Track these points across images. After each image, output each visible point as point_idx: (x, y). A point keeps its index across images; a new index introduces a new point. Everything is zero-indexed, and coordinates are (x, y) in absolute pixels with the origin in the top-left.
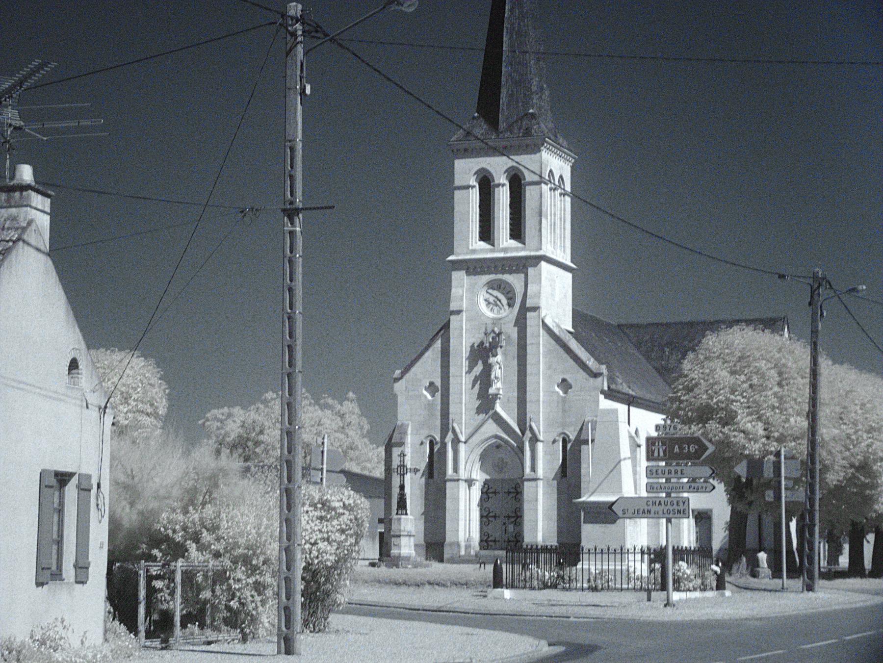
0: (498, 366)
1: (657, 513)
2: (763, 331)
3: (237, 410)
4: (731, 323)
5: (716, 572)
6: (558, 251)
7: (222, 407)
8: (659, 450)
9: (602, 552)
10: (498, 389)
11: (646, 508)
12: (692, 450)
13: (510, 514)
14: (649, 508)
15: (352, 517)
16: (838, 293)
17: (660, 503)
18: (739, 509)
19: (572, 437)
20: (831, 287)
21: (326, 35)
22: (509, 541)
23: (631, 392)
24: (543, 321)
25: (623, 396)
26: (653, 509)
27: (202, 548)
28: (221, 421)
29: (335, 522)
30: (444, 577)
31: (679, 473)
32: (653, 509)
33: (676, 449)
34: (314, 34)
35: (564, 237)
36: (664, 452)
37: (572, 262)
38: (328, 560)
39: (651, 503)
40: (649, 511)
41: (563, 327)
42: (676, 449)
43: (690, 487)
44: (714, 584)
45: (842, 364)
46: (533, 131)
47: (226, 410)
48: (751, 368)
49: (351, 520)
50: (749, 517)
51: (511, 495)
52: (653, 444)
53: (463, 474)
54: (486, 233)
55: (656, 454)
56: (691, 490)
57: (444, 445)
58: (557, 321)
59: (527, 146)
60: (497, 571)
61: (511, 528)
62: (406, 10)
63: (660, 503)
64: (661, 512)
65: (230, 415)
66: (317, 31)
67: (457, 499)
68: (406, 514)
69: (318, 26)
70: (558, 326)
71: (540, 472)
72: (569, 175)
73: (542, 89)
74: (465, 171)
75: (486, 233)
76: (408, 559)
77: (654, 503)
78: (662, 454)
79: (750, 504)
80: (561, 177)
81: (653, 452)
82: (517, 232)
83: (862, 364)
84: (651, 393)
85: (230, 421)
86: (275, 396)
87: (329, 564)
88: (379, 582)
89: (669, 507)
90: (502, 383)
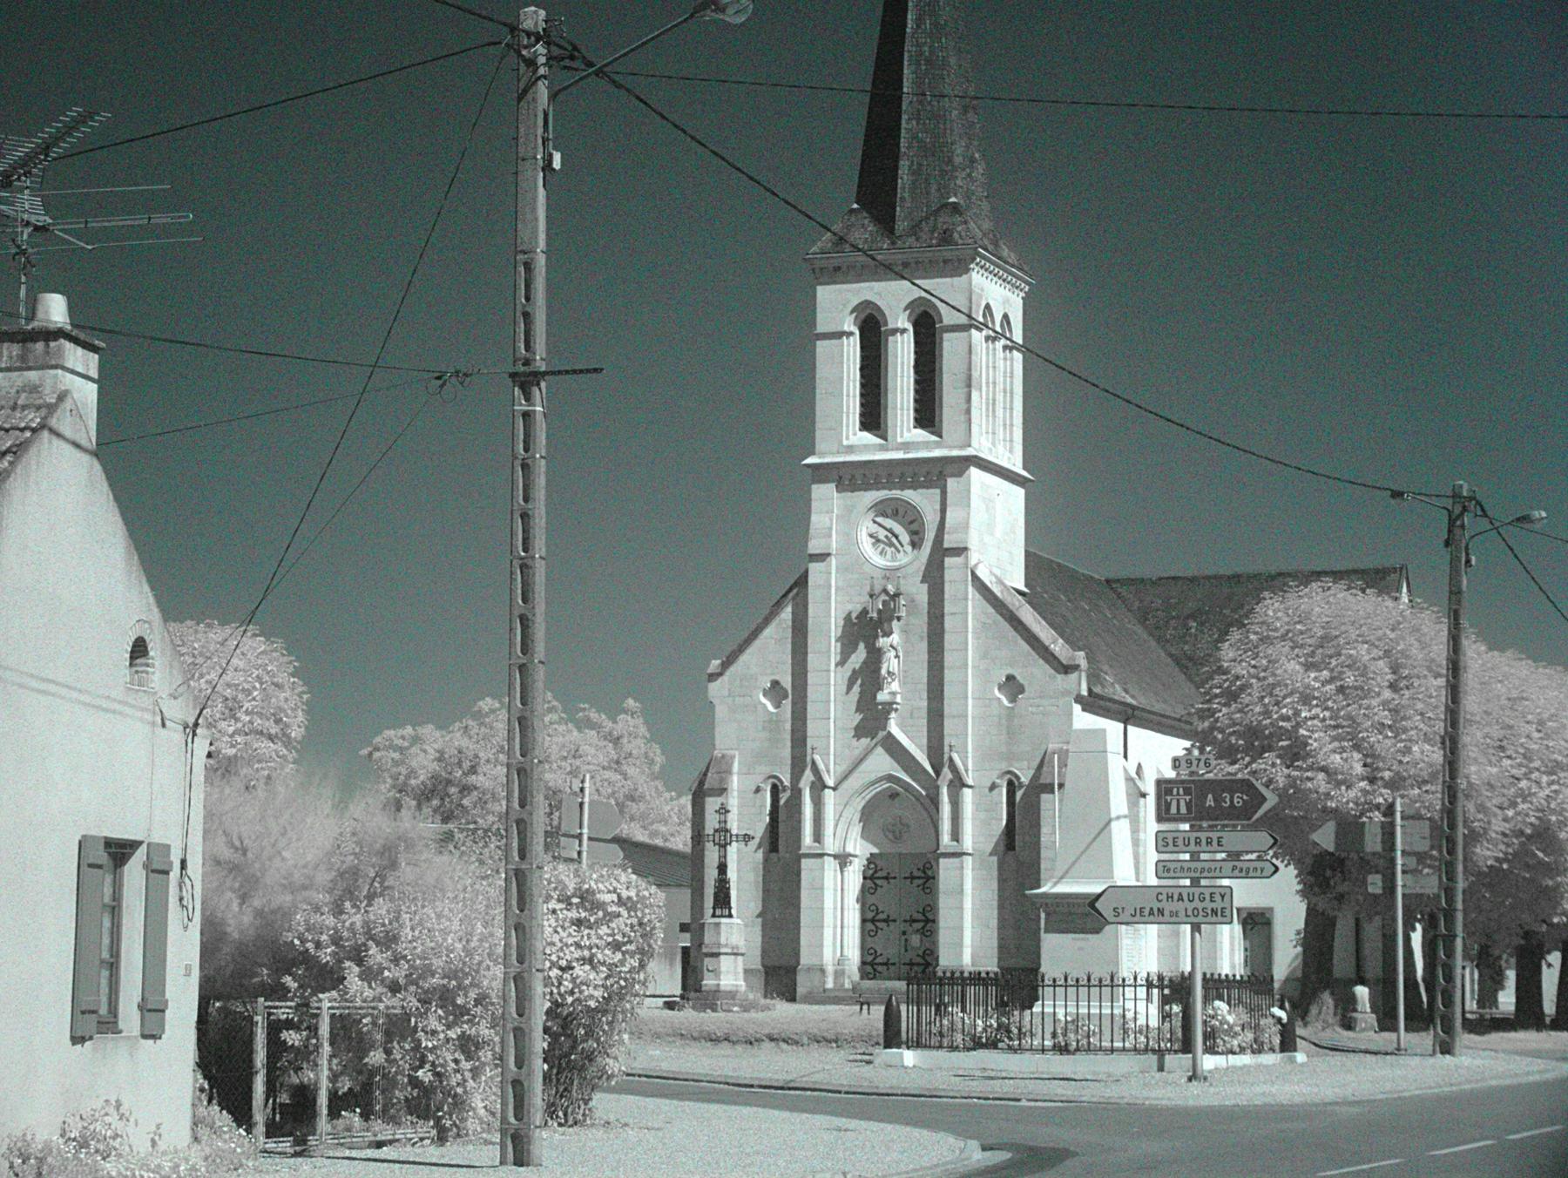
0: (893, 653)
3: (428, 730)
5: (1279, 1020)
7: (402, 726)
8: (1179, 803)
10: (894, 694)
11: (1156, 905)
18: (1320, 907)
19: (1025, 780)
21: (591, 65)
23: (1129, 700)
24: (973, 573)
26: (1168, 907)
29: (604, 930)
31: (1215, 843)
32: (1168, 907)
33: (1210, 801)
34: (567, 62)
36: (1188, 805)
39: (1164, 897)
40: (1161, 912)
41: (1009, 583)
42: (1210, 801)
44: (1277, 1040)
45: (1502, 650)
46: (956, 235)
47: (409, 730)
49: (632, 926)
53: (831, 845)
54: (873, 417)
55: (1173, 810)
56: (1236, 873)
57: (797, 793)
58: (996, 571)
59: (945, 262)
60: (891, 1018)
61: (915, 940)
63: (1181, 898)
65: (416, 740)
66: (572, 58)
68: (730, 916)
69: (575, 48)
71: (968, 843)
73: (973, 160)
74: (836, 304)
75: (873, 417)
76: (732, 995)
78: (1183, 810)
80: (1006, 317)
81: (1168, 805)
82: (927, 414)
87: (592, 1004)
89: (1197, 903)
90: (901, 682)
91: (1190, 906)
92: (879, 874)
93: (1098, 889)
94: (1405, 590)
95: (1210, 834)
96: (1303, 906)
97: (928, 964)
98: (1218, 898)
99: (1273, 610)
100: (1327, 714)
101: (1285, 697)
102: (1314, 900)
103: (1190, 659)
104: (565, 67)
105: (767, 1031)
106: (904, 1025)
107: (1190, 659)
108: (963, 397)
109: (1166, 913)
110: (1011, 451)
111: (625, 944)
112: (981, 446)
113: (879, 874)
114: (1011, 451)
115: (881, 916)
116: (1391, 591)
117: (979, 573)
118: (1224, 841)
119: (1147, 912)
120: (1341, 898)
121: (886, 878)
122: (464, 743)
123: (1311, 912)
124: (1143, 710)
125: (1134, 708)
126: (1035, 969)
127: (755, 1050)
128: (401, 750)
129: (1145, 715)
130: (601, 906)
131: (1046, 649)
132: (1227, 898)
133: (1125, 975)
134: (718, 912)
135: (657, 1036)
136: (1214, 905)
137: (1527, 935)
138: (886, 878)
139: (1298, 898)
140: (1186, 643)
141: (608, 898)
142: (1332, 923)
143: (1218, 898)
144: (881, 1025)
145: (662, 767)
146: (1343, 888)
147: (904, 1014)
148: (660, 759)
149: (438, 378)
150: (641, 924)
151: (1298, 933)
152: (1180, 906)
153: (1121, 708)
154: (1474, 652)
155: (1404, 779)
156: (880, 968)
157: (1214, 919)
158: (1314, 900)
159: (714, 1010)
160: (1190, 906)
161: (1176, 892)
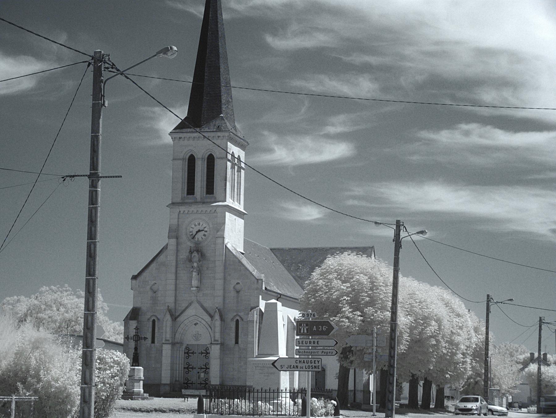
1: (302, 368)
2: (362, 255)
3: (23, 298)
4: (342, 250)
5: (334, 405)
6: (236, 203)
7: (13, 296)
8: (304, 330)
9: (258, 392)
11: (295, 365)
12: (324, 329)
13: (203, 367)
14: (297, 365)
15: (119, 368)
16: (410, 234)
17: (304, 362)
18: (344, 366)
20: (406, 231)
21: (118, 70)
22: (201, 384)
23: (279, 292)
25: (274, 294)
26: (299, 365)
27: (27, 387)
28: (12, 304)
29: (108, 372)
30: (165, 406)
31: (301, 342)
32: (299, 365)
33: (315, 328)
34: (110, 69)
35: (240, 194)
36: (307, 330)
37: (244, 209)
38: (103, 395)
39: (298, 362)
40: (297, 367)
41: (238, 250)
42: (315, 328)
43: (322, 352)
44: (333, 412)
45: (408, 277)
46: (222, 128)
47: (15, 297)
48: (354, 279)
49: (118, 370)
50: (351, 370)
51: (191, 351)
52: (301, 325)
55: (302, 331)
56: (323, 354)
58: (234, 246)
59: (218, 137)
60: (200, 403)
61: (202, 375)
62: (170, 57)
63: (304, 362)
64: (304, 368)
65: (19, 301)
66: (112, 68)
67: (374, 389)
69: (113, 64)
70: (235, 249)
72: (244, 155)
76: (138, 394)
77: (300, 362)
78: (305, 331)
79: (352, 362)
81: (300, 330)
83: (420, 278)
84: (291, 292)
85: (18, 305)
86: (48, 289)
87: (103, 398)
88: (124, 409)
89: (309, 364)
91: (307, 365)
92: (204, 355)
93: (276, 358)
94: (373, 255)
95: (306, 340)
96: (339, 365)
97: (207, 384)
98: (317, 362)
99: (331, 262)
100: (349, 298)
101: (334, 292)
102: (342, 363)
103: (299, 277)
104: (110, 71)
105: (154, 407)
106: (204, 406)
107: (299, 277)
108: (223, 185)
109: (299, 367)
110: (240, 204)
111: (115, 377)
112: (229, 202)
113: (204, 355)
114: (240, 204)
115: (190, 366)
116: (369, 256)
117: (228, 246)
118: (319, 343)
119: (292, 367)
120: (352, 362)
121: (192, 353)
122: (36, 302)
123: (341, 366)
124: (284, 295)
125: (281, 295)
126: (278, 389)
127: (150, 414)
128: (12, 304)
129: (284, 297)
130: (107, 363)
131: (393, 300)
132: (320, 362)
133: (282, 388)
134: (134, 364)
135: (128, 410)
136: (315, 365)
137: (413, 376)
138: (192, 353)
139: (337, 362)
140: (298, 272)
141: (109, 360)
142: (348, 371)
143: (317, 362)
144: (197, 405)
145: (108, 311)
146: (352, 359)
147: (205, 402)
148: (107, 308)
149: (63, 178)
150: (121, 370)
151: (337, 374)
152: (304, 365)
153: (276, 294)
154: (402, 279)
155: (375, 322)
156: (189, 385)
157: (294, 369)
158: (342, 363)
159: (132, 400)
160: (307, 365)
161: (302, 360)
